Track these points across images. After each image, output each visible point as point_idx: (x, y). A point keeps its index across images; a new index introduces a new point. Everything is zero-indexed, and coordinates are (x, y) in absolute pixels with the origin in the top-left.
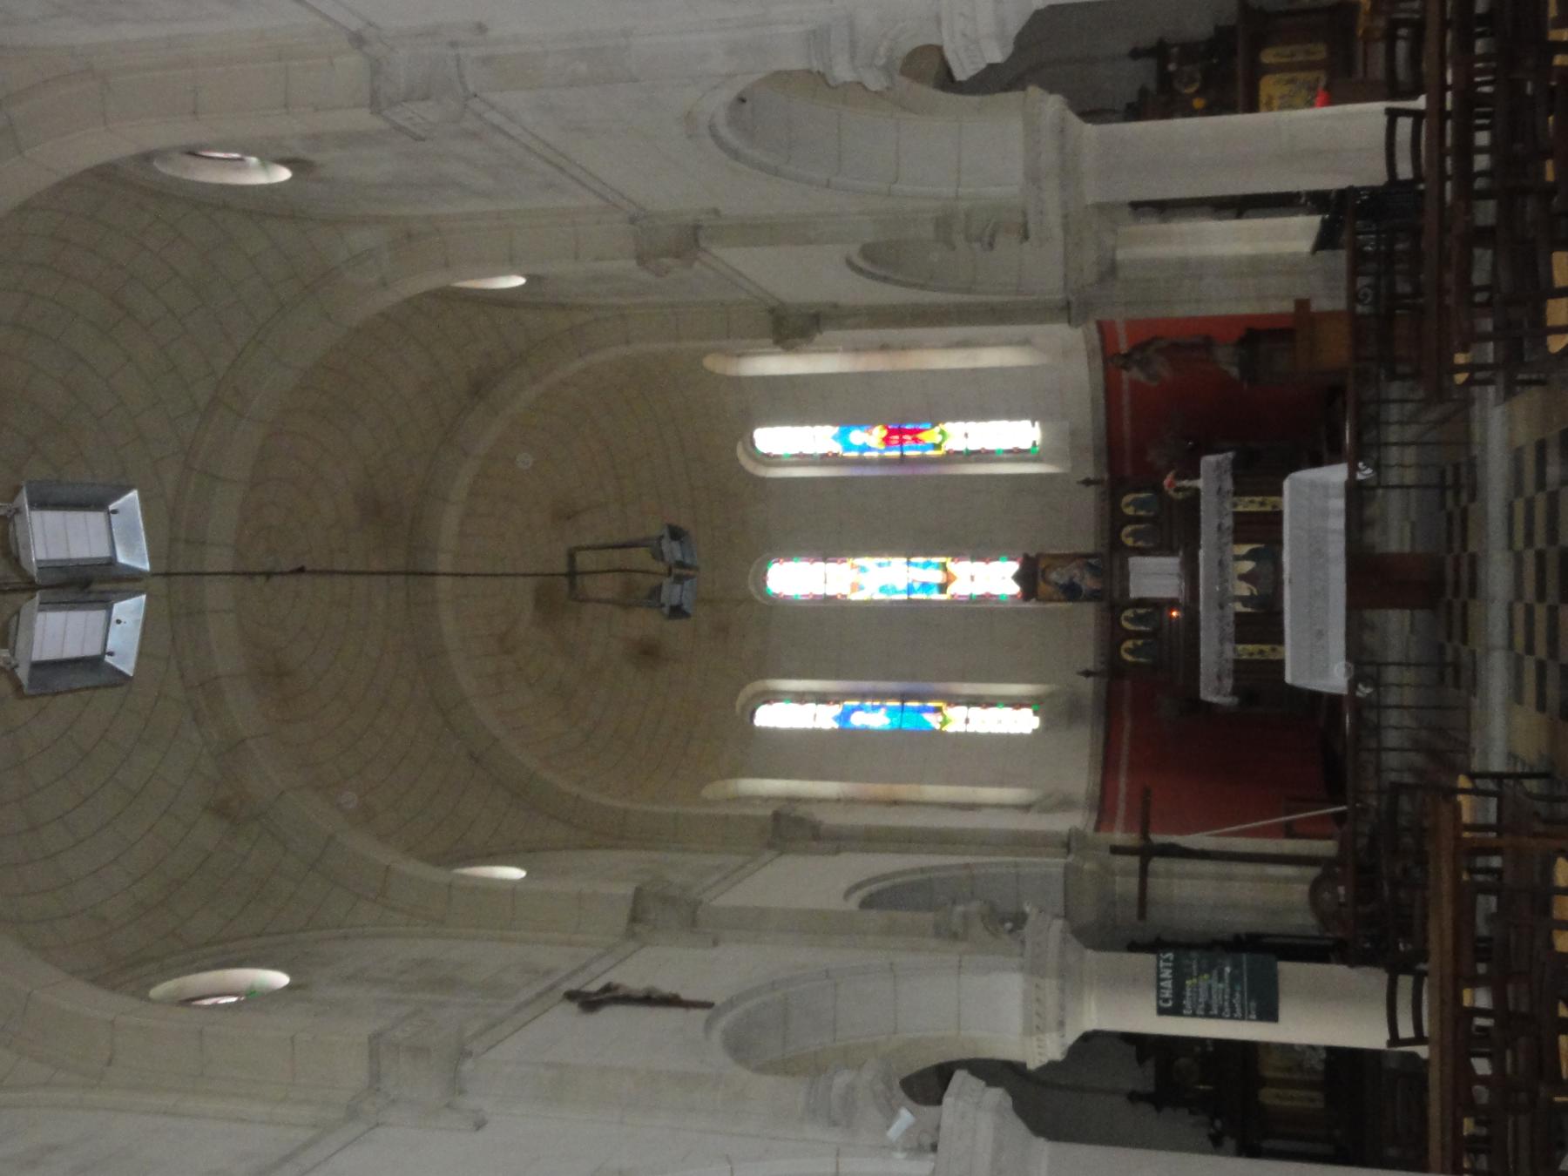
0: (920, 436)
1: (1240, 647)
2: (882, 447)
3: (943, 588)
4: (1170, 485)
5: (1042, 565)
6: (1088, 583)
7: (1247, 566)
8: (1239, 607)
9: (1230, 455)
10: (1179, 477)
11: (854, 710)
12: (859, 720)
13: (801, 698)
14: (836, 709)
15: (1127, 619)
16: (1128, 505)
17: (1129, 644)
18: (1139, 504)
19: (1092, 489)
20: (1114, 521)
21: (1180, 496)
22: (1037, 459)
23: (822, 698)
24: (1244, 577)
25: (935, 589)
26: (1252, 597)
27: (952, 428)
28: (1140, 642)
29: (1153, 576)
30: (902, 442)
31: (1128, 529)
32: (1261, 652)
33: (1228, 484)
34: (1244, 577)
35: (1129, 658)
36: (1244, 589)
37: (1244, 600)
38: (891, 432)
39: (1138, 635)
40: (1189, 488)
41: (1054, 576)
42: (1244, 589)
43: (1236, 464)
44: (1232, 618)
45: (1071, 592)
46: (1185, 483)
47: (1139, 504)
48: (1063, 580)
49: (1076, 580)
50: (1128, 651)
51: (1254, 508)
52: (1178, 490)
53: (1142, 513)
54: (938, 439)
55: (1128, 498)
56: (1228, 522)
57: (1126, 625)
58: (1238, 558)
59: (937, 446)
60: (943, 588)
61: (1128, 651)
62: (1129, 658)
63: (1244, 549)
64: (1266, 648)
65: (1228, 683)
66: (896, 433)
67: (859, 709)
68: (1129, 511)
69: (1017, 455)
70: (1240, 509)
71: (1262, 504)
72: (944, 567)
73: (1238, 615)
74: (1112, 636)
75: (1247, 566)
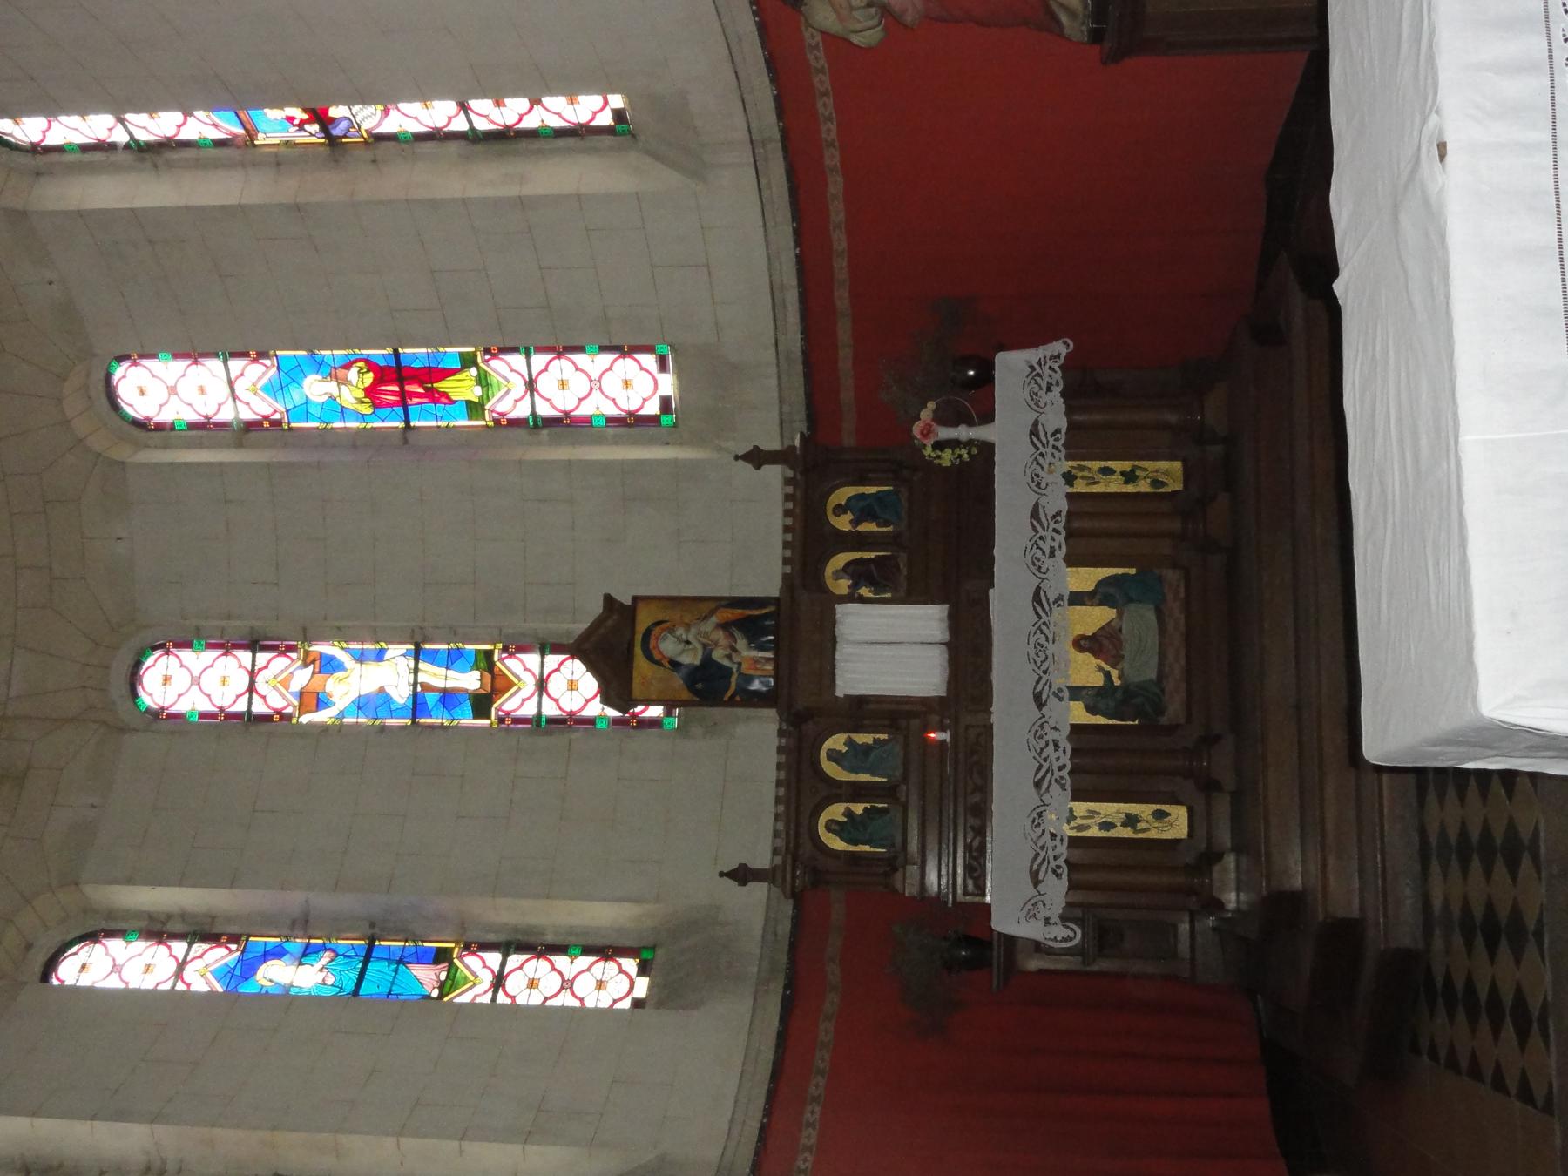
0: (443, 386)
1: (1081, 808)
2: (366, 409)
3: (481, 704)
4: (926, 433)
5: (644, 620)
6: (753, 663)
7: (1096, 618)
8: (1078, 713)
9: (1060, 348)
10: (942, 419)
11: (267, 955)
12: (275, 974)
13: (157, 930)
14: (219, 956)
15: (834, 756)
16: (840, 510)
17: (836, 811)
18: (863, 509)
19: (774, 474)
20: (809, 541)
21: (947, 458)
22: (674, 436)
23: (204, 932)
24: (1082, 644)
25: (467, 708)
26: (1107, 690)
27: (508, 369)
28: (859, 809)
29: (888, 648)
30: (403, 400)
31: (841, 560)
32: (1131, 821)
33: (1056, 417)
34: (1082, 644)
35: (837, 844)
36: (1087, 671)
37: (1094, 698)
38: (383, 375)
39: (856, 792)
40: (970, 443)
41: (668, 647)
42: (1087, 671)
43: (1069, 366)
44: (1062, 737)
45: (707, 687)
46: (963, 432)
47: (863, 509)
48: (691, 658)
49: (718, 655)
50: (832, 826)
51: (1115, 485)
52: (940, 446)
53: (869, 527)
54: (475, 393)
55: (843, 494)
56: (1056, 501)
57: (831, 769)
58: (1077, 599)
59: (475, 408)
60: (481, 704)
61: (832, 826)
62: (837, 844)
63: (1086, 578)
64: (1144, 810)
65: (1056, 891)
66: (399, 381)
67: (278, 953)
68: (843, 523)
69: (632, 423)
70: (1080, 487)
71: (1130, 477)
72: (486, 663)
73: (1077, 729)
74: (802, 787)
75: (1096, 618)
